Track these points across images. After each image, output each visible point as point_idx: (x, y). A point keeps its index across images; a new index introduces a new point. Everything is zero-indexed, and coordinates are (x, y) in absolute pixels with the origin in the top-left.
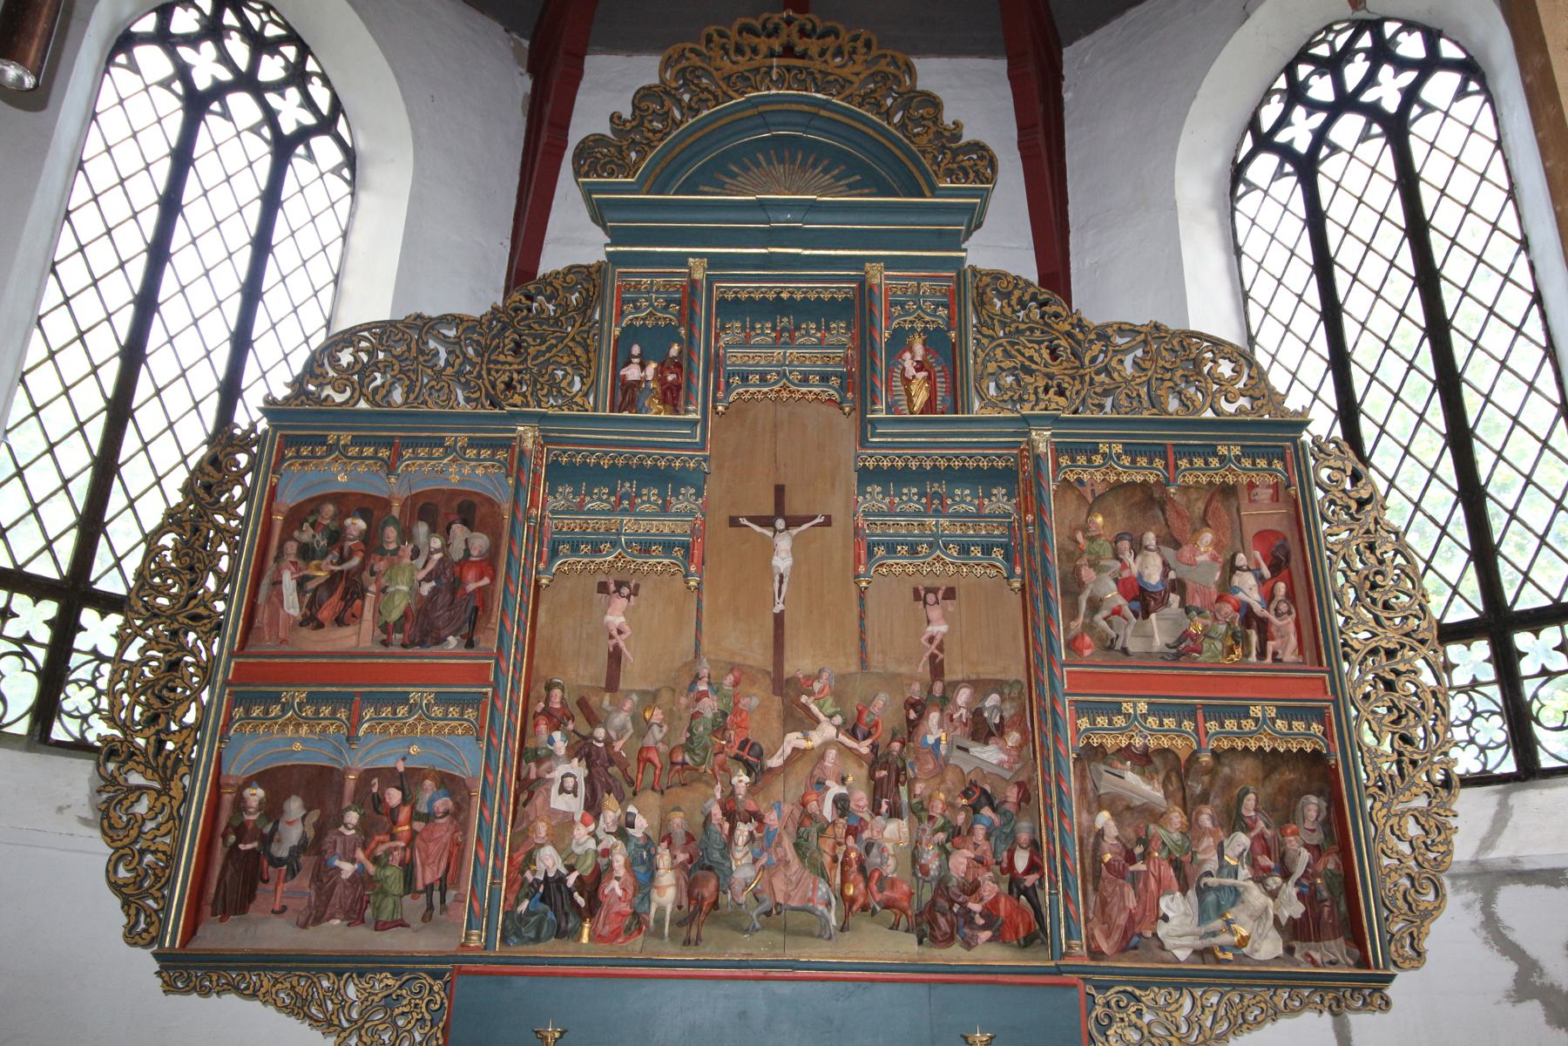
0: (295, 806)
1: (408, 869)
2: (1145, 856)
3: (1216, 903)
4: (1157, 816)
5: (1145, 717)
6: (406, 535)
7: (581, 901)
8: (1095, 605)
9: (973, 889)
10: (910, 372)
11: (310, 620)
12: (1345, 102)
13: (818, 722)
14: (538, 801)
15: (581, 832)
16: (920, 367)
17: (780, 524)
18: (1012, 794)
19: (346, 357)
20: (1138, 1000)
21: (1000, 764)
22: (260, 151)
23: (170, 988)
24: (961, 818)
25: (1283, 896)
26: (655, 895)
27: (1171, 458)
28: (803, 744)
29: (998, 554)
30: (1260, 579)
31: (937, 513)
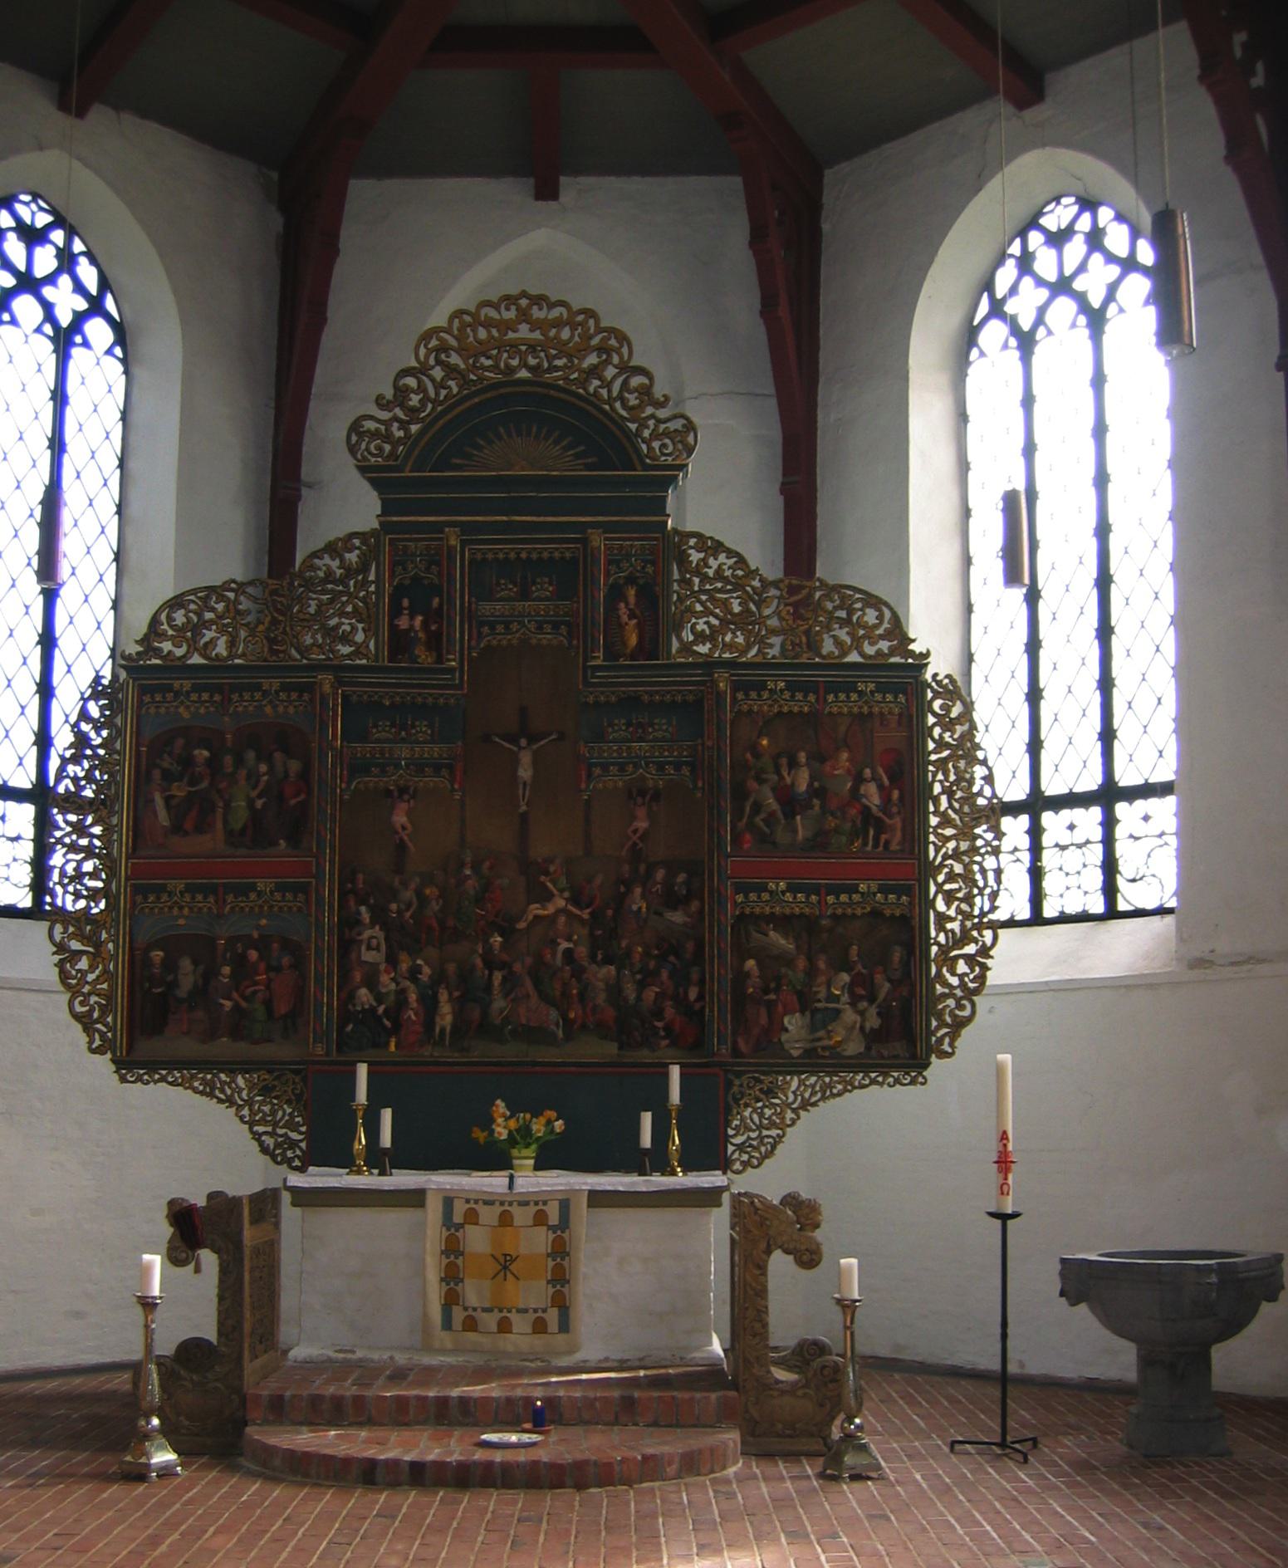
0: (186, 964)
1: (268, 1004)
2: (777, 990)
3: (823, 1019)
4: (790, 963)
5: (783, 893)
6: (239, 761)
7: (387, 1023)
8: (757, 808)
9: (658, 1013)
10: (625, 618)
11: (177, 828)
12: (1062, 286)
13: (553, 895)
14: (354, 956)
15: (385, 978)
16: (632, 616)
17: (523, 742)
18: (690, 946)
19: (180, 617)
20: (761, 1082)
21: (685, 924)
22: (44, 349)
23: (123, 1080)
24: (652, 964)
25: (868, 1015)
26: (438, 1019)
27: (822, 692)
28: (541, 912)
29: (686, 771)
30: (881, 787)
31: (641, 740)
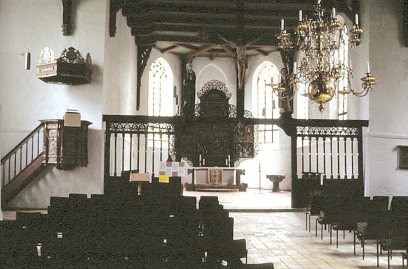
3: (243, 153)
